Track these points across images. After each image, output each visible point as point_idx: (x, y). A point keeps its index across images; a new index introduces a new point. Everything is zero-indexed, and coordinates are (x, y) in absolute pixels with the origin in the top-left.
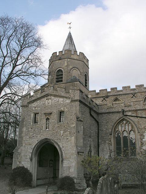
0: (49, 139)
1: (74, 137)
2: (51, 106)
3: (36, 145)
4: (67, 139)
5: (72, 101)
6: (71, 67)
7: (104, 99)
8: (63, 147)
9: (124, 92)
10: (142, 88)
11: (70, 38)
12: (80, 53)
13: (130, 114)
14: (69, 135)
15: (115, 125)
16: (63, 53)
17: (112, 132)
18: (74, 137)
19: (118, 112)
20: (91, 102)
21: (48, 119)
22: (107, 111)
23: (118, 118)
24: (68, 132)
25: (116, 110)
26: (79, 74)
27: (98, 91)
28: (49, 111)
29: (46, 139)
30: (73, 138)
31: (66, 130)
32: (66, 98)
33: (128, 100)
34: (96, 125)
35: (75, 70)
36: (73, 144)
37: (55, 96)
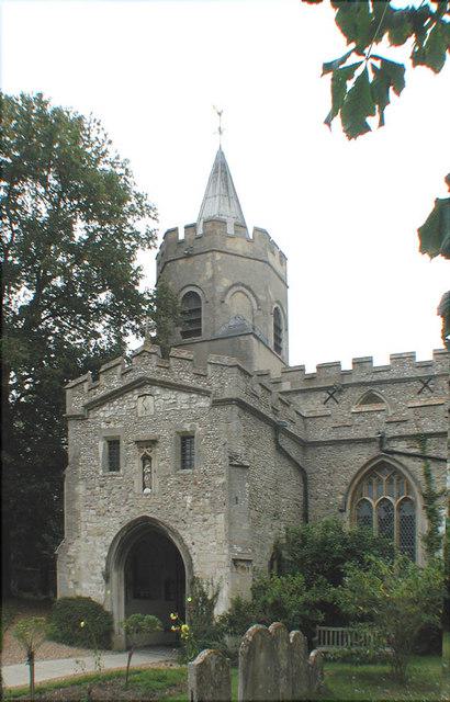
1: (222, 515)
2: (155, 418)
3: (117, 535)
4: (205, 520)
5: (217, 403)
6: (226, 283)
7: (331, 396)
11: (221, 171)
12: (256, 229)
13: (401, 446)
14: (208, 509)
15: (356, 482)
16: (200, 231)
17: (346, 503)
18: (222, 515)
19: (367, 441)
20: (280, 407)
21: (146, 459)
22: (332, 436)
23: (364, 460)
27: (311, 369)
28: (145, 434)
29: (145, 519)
32: (198, 391)
33: (404, 403)
34: (296, 480)
35: (240, 294)
36: (222, 537)
37: (165, 385)
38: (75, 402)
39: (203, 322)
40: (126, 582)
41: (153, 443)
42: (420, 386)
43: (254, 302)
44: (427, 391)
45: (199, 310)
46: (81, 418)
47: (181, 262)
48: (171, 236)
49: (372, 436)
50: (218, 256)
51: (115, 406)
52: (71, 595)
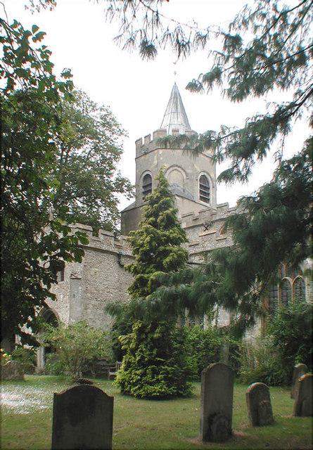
40: (253, 421)
43: (184, 174)
45: (151, 184)
47: (143, 157)
48: (139, 143)
52: (51, 442)
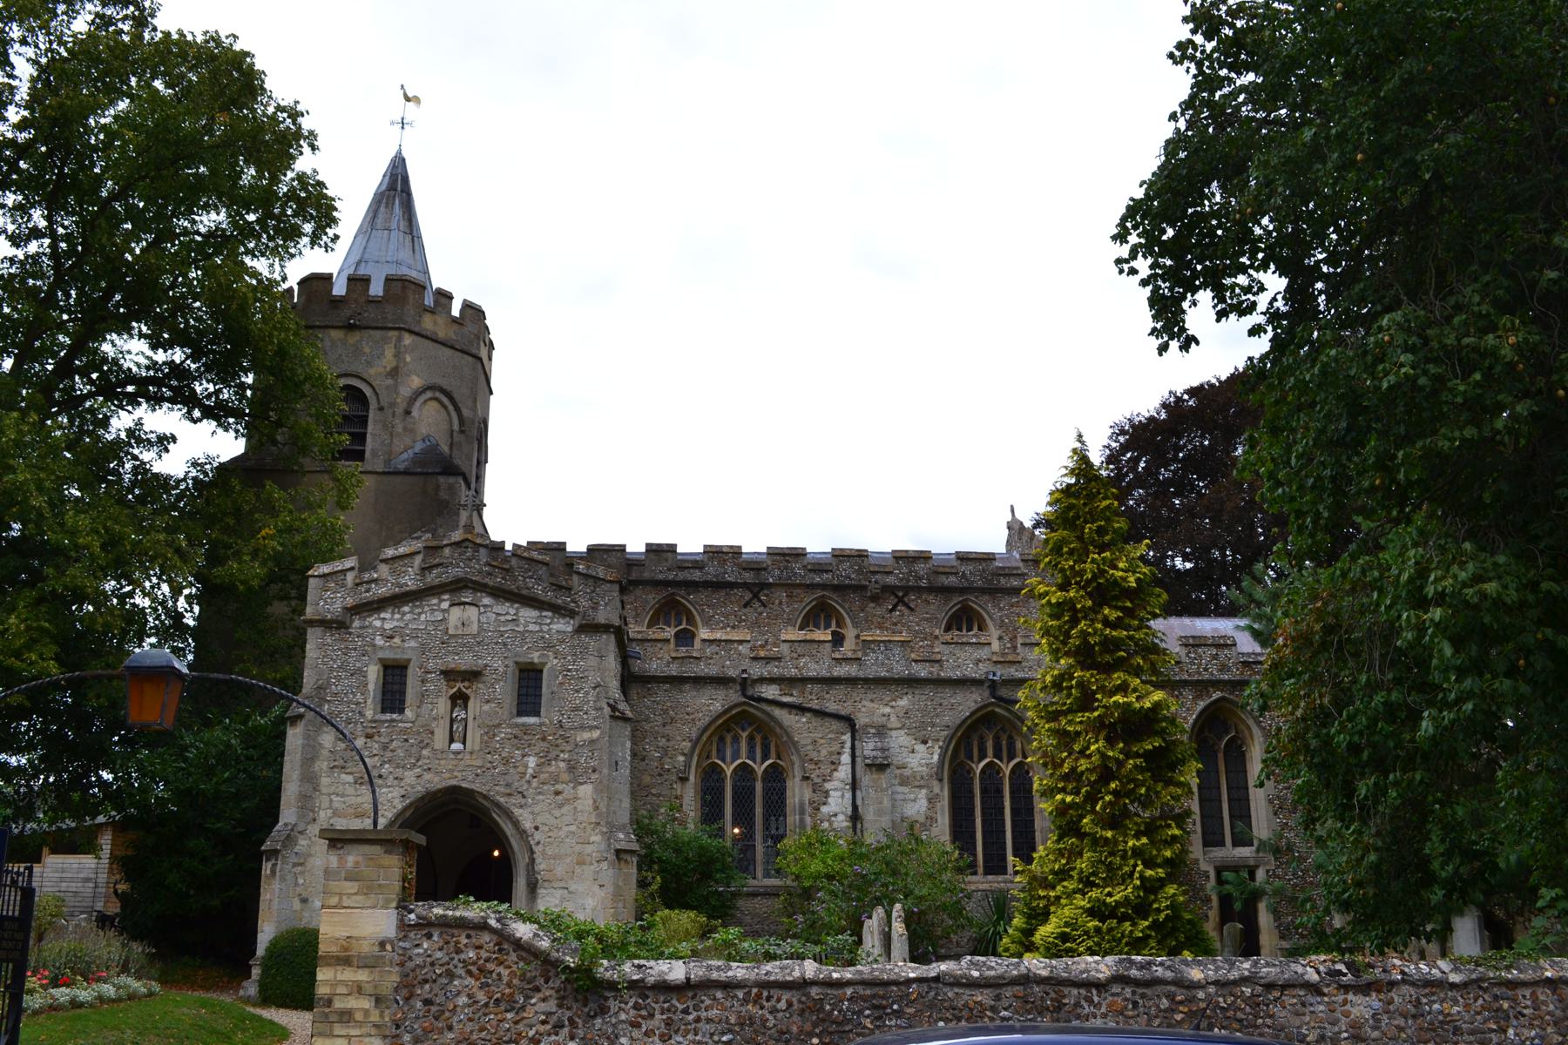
0: (470, 793)
2: (479, 640)
4: (558, 793)
8: (537, 828)
9: (712, 571)
10: (797, 567)
13: (771, 692)
14: (565, 776)
15: (704, 738)
19: (721, 681)
21: (459, 700)
22: (674, 670)
24: (562, 765)
25: (713, 671)
26: (456, 427)
28: (465, 661)
29: (455, 790)
30: (586, 791)
31: (552, 755)
35: (434, 404)
37: (500, 594)
38: (323, 600)
39: (369, 439)
41: (474, 675)
42: (748, 595)
44: (757, 604)
46: (337, 625)
47: (335, 334)
49: (732, 673)
50: (408, 340)
51: (404, 614)
